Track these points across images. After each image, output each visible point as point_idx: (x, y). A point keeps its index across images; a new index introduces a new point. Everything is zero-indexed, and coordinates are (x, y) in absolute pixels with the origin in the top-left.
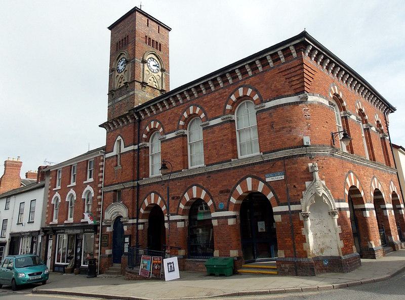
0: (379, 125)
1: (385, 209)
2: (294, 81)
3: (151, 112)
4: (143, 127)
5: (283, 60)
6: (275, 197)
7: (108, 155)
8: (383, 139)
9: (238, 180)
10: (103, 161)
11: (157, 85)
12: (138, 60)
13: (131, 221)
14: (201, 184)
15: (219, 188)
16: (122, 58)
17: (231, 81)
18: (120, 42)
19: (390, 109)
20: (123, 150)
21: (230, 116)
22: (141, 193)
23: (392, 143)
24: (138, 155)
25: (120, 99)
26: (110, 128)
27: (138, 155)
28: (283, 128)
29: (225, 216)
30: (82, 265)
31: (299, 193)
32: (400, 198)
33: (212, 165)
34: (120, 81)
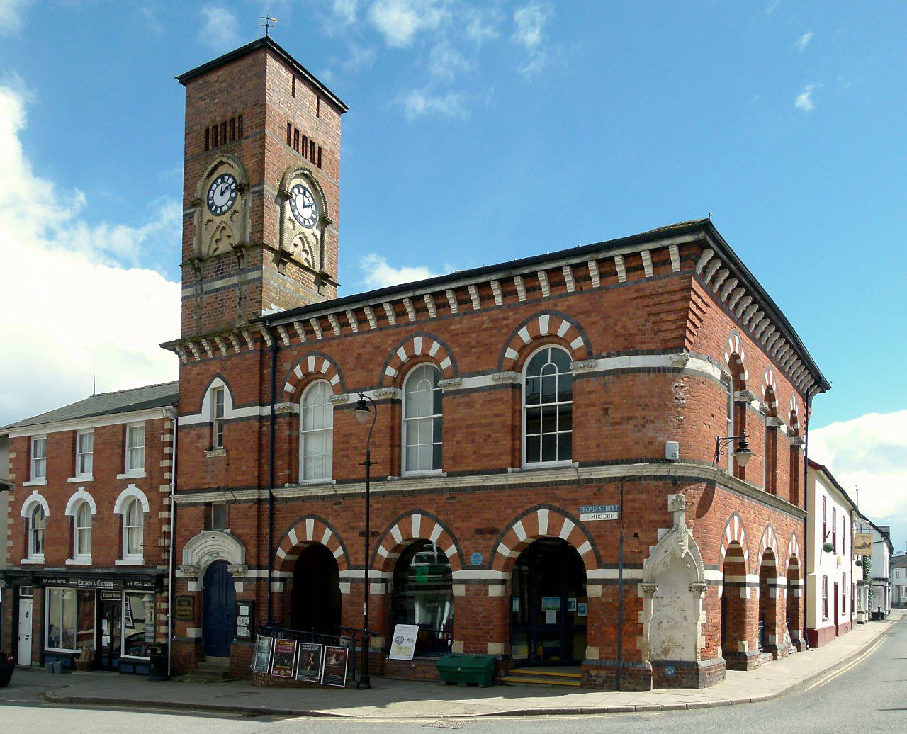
0: (794, 420)
1: (775, 586)
2: (665, 322)
3: (310, 332)
4: (286, 366)
5: (649, 272)
6: (595, 551)
7: (184, 421)
8: (794, 449)
9: (520, 511)
10: (171, 431)
11: (310, 258)
12: (271, 190)
13: (253, 574)
14: (432, 511)
15: (475, 522)
16: (222, 177)
17: (522, 296)
18: (216, 127)
19: (820, 384)
20: (230, 413)
21: (512, 374)
22: (278, 515)
23: (808, 457)
24: (273, 431)
25: (219, 284)
26: (190, 354)
27: (273, 431)
28: (630, 418)
29: (483, 578)
30: (123, 656)
31: (643, 548)
32: (801, 566)
33: (462, 474)
34: (217, 236)
